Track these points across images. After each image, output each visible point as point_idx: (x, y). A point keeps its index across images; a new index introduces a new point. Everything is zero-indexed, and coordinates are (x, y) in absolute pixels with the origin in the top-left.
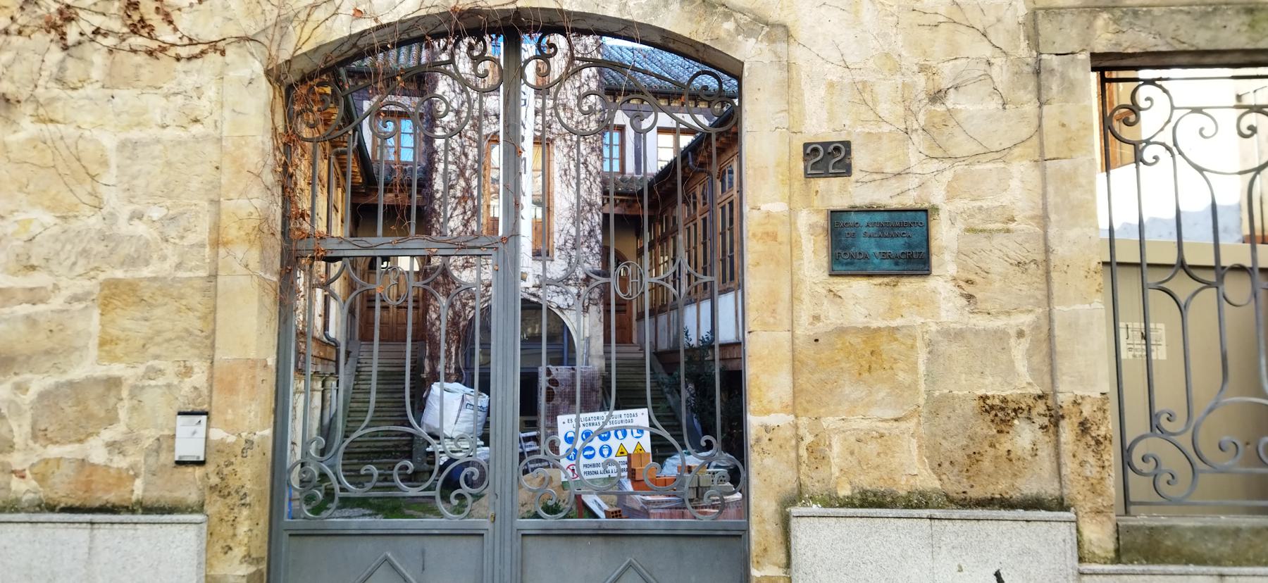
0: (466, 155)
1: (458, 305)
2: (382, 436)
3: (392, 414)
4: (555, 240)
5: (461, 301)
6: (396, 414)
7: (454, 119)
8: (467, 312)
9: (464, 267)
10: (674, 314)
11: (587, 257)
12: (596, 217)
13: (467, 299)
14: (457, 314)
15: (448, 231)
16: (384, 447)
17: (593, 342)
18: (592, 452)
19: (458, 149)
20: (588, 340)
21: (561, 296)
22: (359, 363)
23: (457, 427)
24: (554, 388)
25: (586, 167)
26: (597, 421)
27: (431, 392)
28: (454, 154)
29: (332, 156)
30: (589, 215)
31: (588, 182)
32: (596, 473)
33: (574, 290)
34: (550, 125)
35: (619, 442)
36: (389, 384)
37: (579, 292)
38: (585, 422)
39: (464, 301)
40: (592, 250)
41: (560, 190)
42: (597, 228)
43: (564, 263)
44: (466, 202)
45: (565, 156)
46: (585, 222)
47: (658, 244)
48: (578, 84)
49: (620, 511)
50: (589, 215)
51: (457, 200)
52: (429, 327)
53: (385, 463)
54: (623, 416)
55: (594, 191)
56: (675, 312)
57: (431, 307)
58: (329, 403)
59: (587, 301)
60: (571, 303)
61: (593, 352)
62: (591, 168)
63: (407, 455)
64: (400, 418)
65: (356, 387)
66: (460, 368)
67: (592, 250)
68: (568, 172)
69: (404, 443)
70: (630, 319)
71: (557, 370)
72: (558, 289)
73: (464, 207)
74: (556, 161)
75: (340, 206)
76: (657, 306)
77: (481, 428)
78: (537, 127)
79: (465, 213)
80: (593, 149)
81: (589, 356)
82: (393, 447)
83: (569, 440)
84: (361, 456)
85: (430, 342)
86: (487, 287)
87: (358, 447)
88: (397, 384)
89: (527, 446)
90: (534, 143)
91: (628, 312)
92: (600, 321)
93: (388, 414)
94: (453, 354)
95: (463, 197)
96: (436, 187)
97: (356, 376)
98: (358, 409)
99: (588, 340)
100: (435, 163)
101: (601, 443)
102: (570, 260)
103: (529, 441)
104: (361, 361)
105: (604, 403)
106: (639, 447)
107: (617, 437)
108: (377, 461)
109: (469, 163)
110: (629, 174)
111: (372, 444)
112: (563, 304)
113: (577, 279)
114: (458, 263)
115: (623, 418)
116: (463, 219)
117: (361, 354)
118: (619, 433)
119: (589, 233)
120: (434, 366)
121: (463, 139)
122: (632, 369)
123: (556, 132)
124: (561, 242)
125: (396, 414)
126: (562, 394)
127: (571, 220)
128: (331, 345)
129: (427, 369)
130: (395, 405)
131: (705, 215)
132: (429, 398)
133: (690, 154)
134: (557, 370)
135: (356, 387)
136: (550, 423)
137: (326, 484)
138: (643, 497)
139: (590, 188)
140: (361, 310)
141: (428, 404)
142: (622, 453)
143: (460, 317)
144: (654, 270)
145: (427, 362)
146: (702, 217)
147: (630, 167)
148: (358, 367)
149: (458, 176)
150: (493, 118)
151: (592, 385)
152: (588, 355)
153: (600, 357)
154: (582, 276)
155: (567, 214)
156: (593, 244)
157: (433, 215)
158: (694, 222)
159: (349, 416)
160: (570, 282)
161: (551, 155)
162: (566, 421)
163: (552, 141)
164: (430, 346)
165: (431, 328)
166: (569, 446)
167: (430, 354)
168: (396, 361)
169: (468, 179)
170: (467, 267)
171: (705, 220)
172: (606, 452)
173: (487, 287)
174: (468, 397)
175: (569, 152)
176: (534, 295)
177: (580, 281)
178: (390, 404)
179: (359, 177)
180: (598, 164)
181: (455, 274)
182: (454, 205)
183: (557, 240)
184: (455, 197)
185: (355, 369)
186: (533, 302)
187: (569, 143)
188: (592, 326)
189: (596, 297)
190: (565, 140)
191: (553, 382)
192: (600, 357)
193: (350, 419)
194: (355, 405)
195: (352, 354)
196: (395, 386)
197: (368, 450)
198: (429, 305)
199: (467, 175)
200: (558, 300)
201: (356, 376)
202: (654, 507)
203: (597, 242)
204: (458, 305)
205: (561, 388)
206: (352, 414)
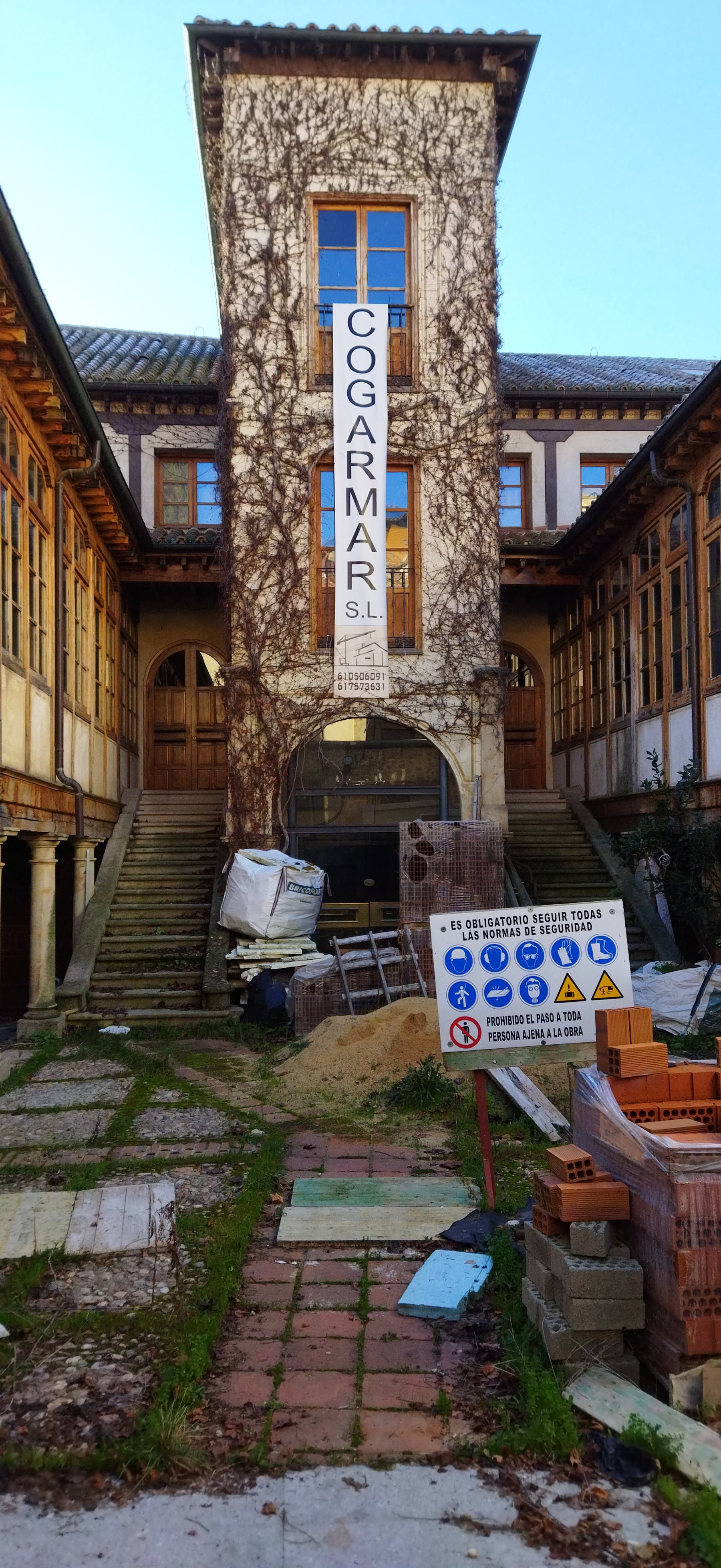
0: (282, 490)
1: (275, 729)
2: (162, 934)
3: (179, 898)
4: (424, 621)
5: (279, 723)
6: (186, 899)
7: (262, 432)
8: (289, 739)
9: (283, 668)
10: (619, 739)
11: (476, 647)
12: (490, 581)
13: (289, 719)
14: (273, 743)
15: (257, 612)
16: (164, 951)
17: (487, 784)
18: (504, 993)
19: (270, 480)
20: (480, 781)
21: (435, 712)
22: (136, 821)
23: (274, 920)
24: (425, 856)
25: (473, 501)
26: (514, 927)
27: (234, 864)
28: (263, 488)
29: (61, 483)
30: (478, 579)
31: (476, 525)
32: (514, 1036)
33: (453, 701)
34: (414, 435)
35: (562, 972)
36: (180, 852)
37: (463, 704)
38: (489, 929)
39: (284, 722)
40: (483, 635)
41: (431, 539)
42: (492, 599)
43: (439, 658)
44: (283, 566)
45: (437, 483)
46: (471, 590)
47: (587, 630)
48: (457, 366)
49: (587, 1162)
50: (478, 579)
51: (269, 563)
52: (230, 763)
53: (163, 978)
54: (569, 916)
55: (487, 539)
56: (621, 735)
57: (234, 732)
58: (82, 883)
59: (476, 718)
60: (451, 722)
61: (488, 799)
62: (480, 501)
63: (198, 964)
64: (191, 905)
65: (130, 857)
66: (280, 827)
67: (483, 635)
68: (443, 511)
69: (195, 944)
70: (543, 754)
71: (430, 826)
72: (430, 701)
73: (281, 574)
74: (423, 493)
75: (91, 578)
76: (588, 729)
77: (314, 921)
78: (393, 439)
79: (281, 582)
80: (483, 471)
81: (482, 806)
82: (177, 951)
83: (459, 966)
84: (127, 965)
85: (233, 787)
86: (318, 699)
87: (125, 952)
88: (191, 852)
89: (383, 956)
90: (388, 466)
91: (538, 743)
92: (498, 749)
93: (174, 899)
94: (270, 805)
95: (279, 556)
96: (236, 542)
97: (131, 840)
98: (130, 891)
99: (480, 781)
100: (233, 504)
101: (524, 973)
102: (448, 652)
103: (386, 946)
104: (140, 818)
105: (508, 880)
106: (606, 982)
107: (557, 959)
108: (151, 974)
109: (287, 501)
110: (538, 529)
111: (145, 947)
112: (438, 725)
113: (461, 682)
114: (273, 663)
115: (570, 920)
116: (279, 592)
117: (142, 808)
118: (563, 953)
119: (479, 608)
120: (239, 823)
121: (277, 464)
122: (550, 828)
123: (423, 445)
124: (434, 623)
125: (186, 899)
126: (441, 870)
127: (449, 588)
128: (68, 790)
129: (230, 829)
130: (187, 884)
131: (676, 565)
132: (231, 874)
133: (652, 454)
134: (430, 826)
135: (130, 857)
136: (420, 916)
137: (68, 1012)
138: (653, 1137)
139: (479, 535)
140: (146, 745)
141: (229, 882)
142: (569, 994)
143: (278, 746)
144: (581, 673)
145: (229, 818)
146: (670, 569)
147: (539, 519)
148: (134, 828)
149: (270, 524)
150: (323, 427)
151: (490, 853)
152: (480, 804)
153: (500, 808)
154: (468, 678)
155: (442, 577)
156: (484, 626)
157: (233, 586)
158: (654, 581)
159: (115, 902)
160: (450, 688)
161: (416, 483)
162: (448, 927)
163: (417, 460)
164: (233, 793)
165: (235, 764)
166: (454, 979)
167: (234, 805)
168: (186, 818)
169: (286, 527)
170: (287, 668)
171: (675, 573)
172: (534, 993)
173: (318, 699)
174: (290, 872)
175: (444, 477)
176: (392, 710)
177: (465, 686)
178: (178, 883)
179: (121, 534)
180: (492, 494)
181: (270, 678)
182: (265, 570)
183: (428, 620)
184: (265, 557)
185: (128, 831)
186: (391, 722)
187: (444, 462)
188: (485, 760)
189: (492, 712)
190: (451, 301)
191: (426, 847)
192: (500, 808)
193: (115, 906)
194: (126, 884)
195: (125, 809)
196: (189, 856)
197: (141, 955)
198: (230, 729)
199: (284, 520)
200: (431, 718)
201: (131, 840)
202: (688, 1167)
203: (492, 621)
204: (275, 729)
205: (437, 857)
206: (120, 899)
